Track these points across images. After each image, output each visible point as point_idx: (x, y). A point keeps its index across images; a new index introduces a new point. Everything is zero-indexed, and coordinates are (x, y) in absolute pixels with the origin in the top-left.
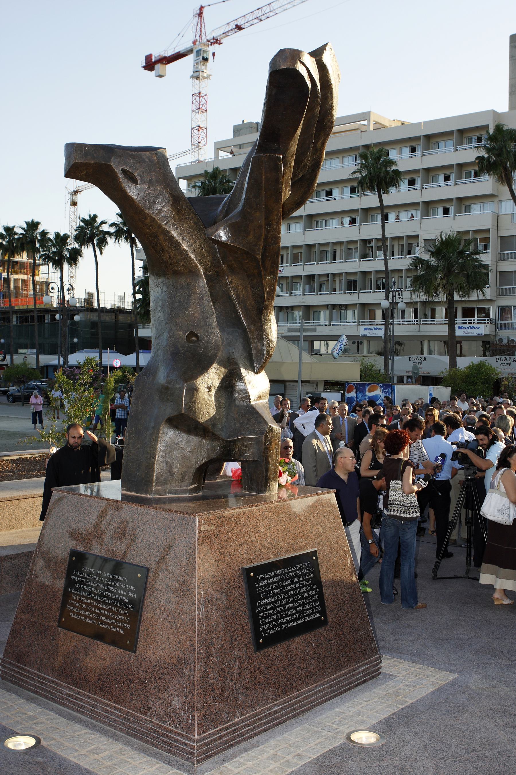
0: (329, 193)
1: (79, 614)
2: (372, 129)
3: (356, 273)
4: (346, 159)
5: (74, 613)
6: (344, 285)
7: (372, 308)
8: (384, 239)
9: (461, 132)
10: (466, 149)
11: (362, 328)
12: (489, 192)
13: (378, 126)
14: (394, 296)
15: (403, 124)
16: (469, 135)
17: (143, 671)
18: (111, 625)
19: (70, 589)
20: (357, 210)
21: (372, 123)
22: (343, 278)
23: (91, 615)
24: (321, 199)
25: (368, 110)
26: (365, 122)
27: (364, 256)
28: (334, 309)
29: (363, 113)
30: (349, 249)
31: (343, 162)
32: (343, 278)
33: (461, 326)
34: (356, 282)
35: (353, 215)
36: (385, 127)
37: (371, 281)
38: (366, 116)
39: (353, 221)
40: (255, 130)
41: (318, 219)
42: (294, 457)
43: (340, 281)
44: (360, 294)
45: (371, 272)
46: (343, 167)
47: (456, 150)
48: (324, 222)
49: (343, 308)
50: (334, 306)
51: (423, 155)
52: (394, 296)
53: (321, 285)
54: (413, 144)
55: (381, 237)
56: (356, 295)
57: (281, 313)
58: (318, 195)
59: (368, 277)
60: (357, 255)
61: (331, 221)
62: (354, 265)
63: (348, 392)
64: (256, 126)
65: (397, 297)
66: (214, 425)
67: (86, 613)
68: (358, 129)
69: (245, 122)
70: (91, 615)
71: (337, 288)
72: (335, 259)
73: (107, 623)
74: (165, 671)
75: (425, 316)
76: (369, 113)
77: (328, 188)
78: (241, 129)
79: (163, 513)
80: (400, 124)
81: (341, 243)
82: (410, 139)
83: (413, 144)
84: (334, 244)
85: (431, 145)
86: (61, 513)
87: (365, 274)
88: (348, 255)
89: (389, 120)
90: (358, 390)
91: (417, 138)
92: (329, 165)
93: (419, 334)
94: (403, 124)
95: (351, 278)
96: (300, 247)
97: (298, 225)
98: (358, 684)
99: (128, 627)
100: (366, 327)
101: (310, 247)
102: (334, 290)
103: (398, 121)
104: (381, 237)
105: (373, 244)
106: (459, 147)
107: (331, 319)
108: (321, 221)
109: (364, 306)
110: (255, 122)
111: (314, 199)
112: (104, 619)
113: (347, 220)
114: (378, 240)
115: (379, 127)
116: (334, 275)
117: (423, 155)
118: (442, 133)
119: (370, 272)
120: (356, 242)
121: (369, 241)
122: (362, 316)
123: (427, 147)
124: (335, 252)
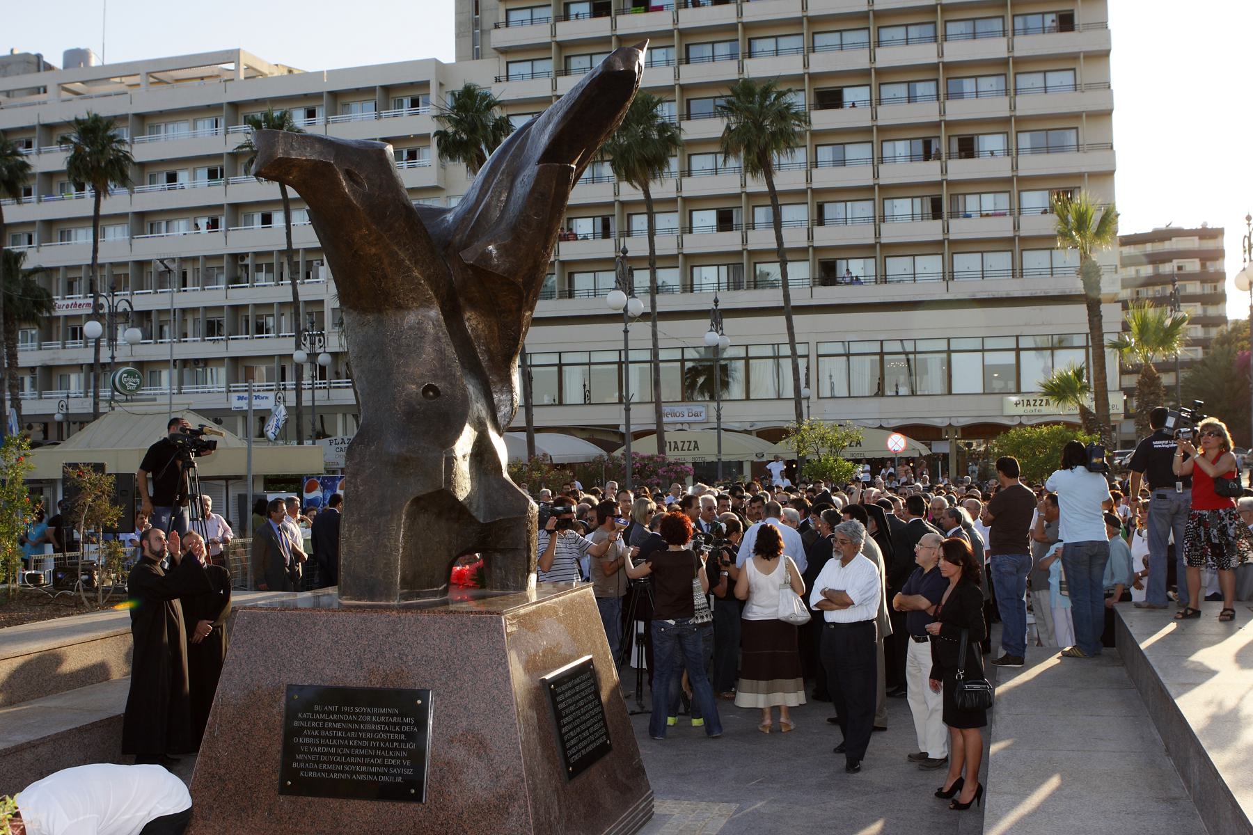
0: (172, 178)
1: (318, 771)
2: (242, 77)
3: (221, 308)
4: (200, 124)
5: (307, 770)
6: (202, 327)
7: (249, 364)
8: (290, 252)
9: (387, 89)
10: (395, 116)
11: (234, 396)
12: (432, 182)
13: (252, 73)
14: (313, 344)
15: (290, 71)
16: (398, 95)
17: (442, 824)
18: (378, 774)
19: (295, 740)
20: (221, 207)
21: (242, 67)
22: (200, 316)
23: (340, 768)
24: (159, 186)
25: (236, 47)
26: (231, 66)
27: (234, 280)
28: (185, 367)
29: (227, 52)
30: (208, 269)
31: (195, 128)
32: (200, 316)
33: (241, 394)
34: (220, 325)
35: (213, 214)
36: (262, 74)
37: (247, 321)
38: (232, 56)
39: (213, 224)
40: (35, 67)
41: (153, 219)
42: (801, 500)
43: (194, 321)
44: (230, 342)
45: (247, 306)
46: (195, 136)
47: (379, 117)
48: (164, 225)
49: (201, 365)
50: (185, 362)
51: (328, 122)
52: (313, 344)
53: (161, 328)
54: (310, 104)
55: (285, 247)
56: (224, 343)
57: (186, 371)
58: (152, 181)
59: (242, 313)
60: (223, 278)
61: (176, 223)
62: (218, 295)
63: (309, 491)
64: (35, 60)
65: (317, 345)
66: (471, 504)
67: (331, 767)
68: (217, 76)
69: (16, 52)
70: (340, 768)
71: (190, 332)
72: (185, 285)
73: (373, 774)
74: (478, 817)
75: (337, 375)
76: (238, 51)
77: (171, 169)
78: (9, 64)
79: (446, 617)
80: (286, 73)
81: (195, 259)
82: (306, 97)
83: (310, 104)
84: (184, 260)
85: (339, 107)
86: (257, 640)
87: (236, 308)
88: (208, 279)
89: (270, 65)
90: (325, 487)
91: (318, 96)
92: (170, 133)
93: (328, 403)
94: (290, 71)
95: (213, 316)
96: (125, 264)
97: (119, 229)
98: (641, 826)
99: (410, 772)
100: (241, 394)
101: (141, 265)
102: (185, 336)
103: (283, 66)
104: (285, 247)
105: (248, 261)
106: (384, 113)
107: (181, 383)
108: (159, 224)
109: (235, 361)
110: (33, 52)
111: (147, 187)
112: (364, 769)
113: (202, 223)
114: (281, 252)
115: (254, 75)
116: (184, 311)
117: (328, 122)
118: (358, 89)
119: (246, 306)
120: (220, 257)
121: (243, 256)
122: (233, 378)
123: (333, 111)
124: (185, 274)
